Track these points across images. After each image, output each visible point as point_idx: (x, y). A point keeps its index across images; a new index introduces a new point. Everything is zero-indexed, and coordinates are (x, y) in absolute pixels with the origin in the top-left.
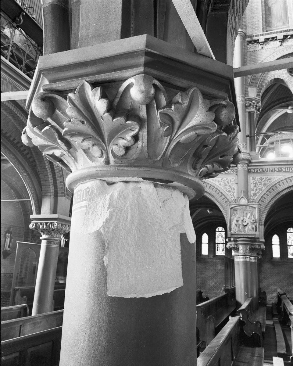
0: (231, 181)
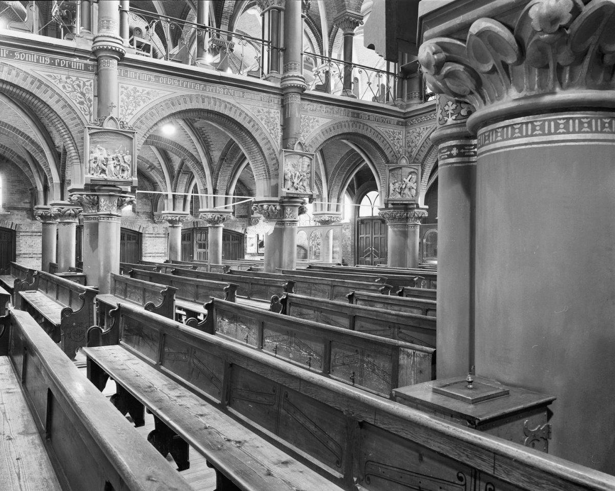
0: (84, 83)
